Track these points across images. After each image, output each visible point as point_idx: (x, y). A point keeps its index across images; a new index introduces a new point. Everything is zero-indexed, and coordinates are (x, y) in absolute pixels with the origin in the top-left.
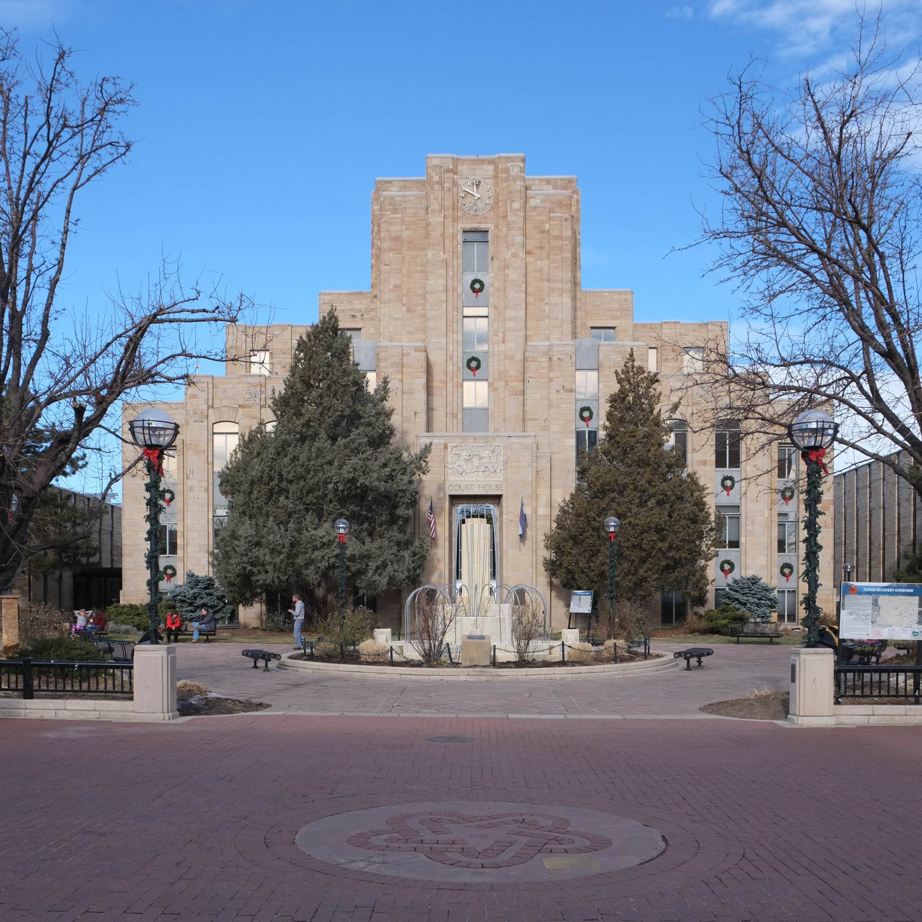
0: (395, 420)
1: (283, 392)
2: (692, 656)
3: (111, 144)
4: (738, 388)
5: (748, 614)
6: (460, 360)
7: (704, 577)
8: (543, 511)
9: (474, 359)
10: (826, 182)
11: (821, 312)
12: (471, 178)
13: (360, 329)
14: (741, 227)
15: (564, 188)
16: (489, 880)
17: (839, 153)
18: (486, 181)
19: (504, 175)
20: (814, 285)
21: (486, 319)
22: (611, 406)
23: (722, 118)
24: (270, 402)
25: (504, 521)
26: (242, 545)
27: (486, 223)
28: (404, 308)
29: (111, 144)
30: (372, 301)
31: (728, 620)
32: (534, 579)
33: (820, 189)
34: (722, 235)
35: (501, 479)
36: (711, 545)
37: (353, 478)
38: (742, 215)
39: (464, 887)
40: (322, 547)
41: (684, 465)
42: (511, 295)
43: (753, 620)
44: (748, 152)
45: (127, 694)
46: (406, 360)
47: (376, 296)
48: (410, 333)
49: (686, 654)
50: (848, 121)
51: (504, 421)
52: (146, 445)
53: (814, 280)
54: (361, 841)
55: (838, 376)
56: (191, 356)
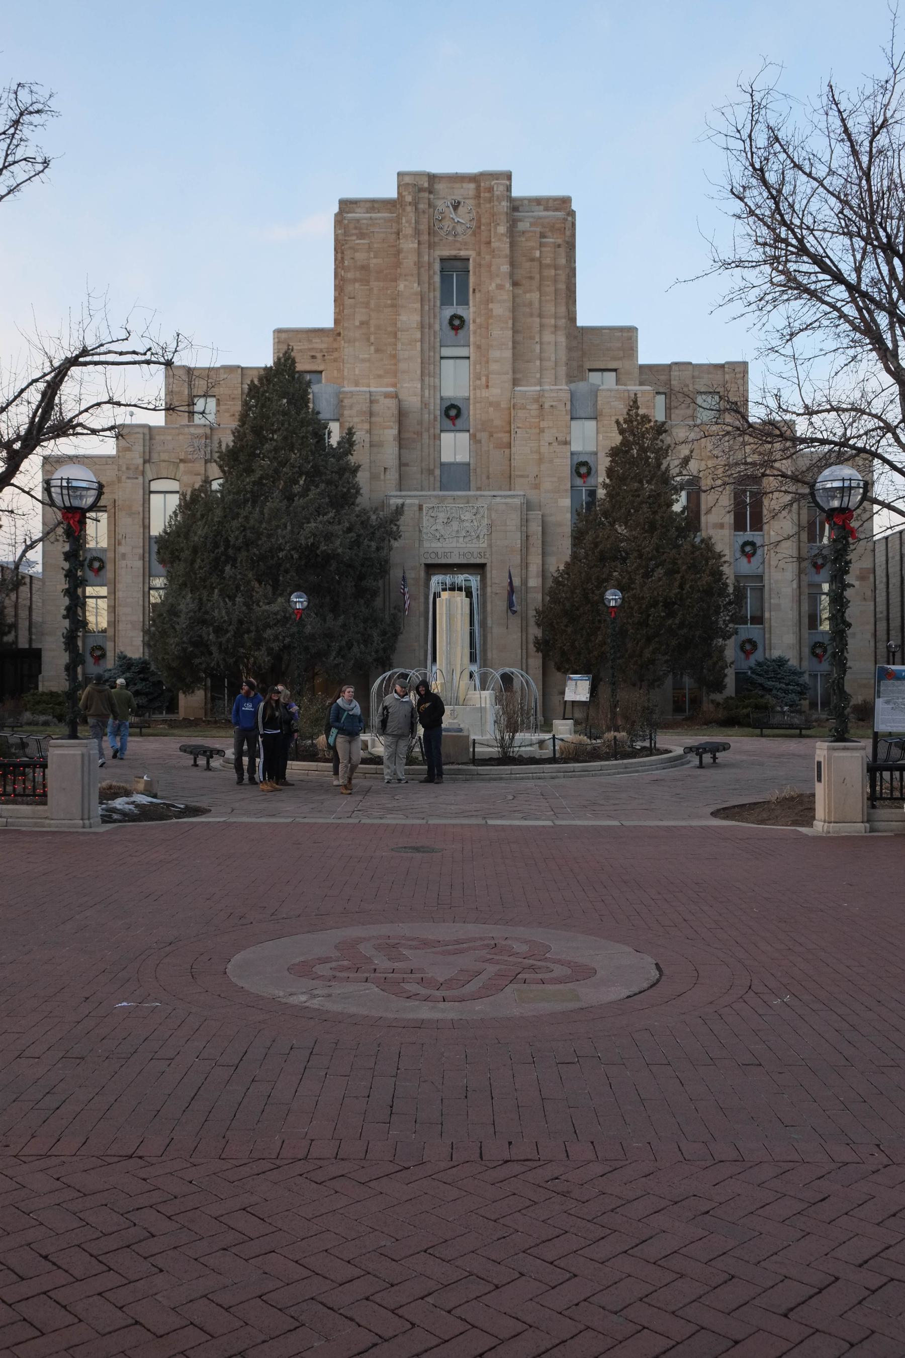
0: (362, 478)
1: (231, 444)
2: (705, 751)
3: (25, 159)
4: (751, 440)
5: (773, 701)
6: (438, 407)
7: (721, 658)
8: (534, 582)
9: (453, 406)
10: (854, 202)
11: (851, 352)
12: (450, 198)
13: (321, 372)
14: (757, 254)
15: (557, 210)
16: (452, 1015)
17: (869, 169)
18: (467, 201)
19: (487, 195)
20: (842, 320)
21: (467, 361)
22: (611, 461)
23: (732, 131)
24: (216, 456)
25: (489, 594)
26: (183, 622)
27: (467, 249)
28: (372, 348)
29: (25, 159)
30: (335, 340)
31: (749, 709)
32: (524, 661)
33: (847, 212)
34: (733, 265)
35: (485, 545)
36: (730, 621)
37: (312, 544)
38: (756, 241)
39: (420, 1025)
40: (275, 625)
41: (698, 529)
42: (496, 332)
43: (779, 709)
44: (761, 170)
45: (40, 797)
46: (376, 408)
47: (339, 334)
48: (380, 376)
49: (698, 749)
50: (878, 133)
51: (488, 478)
52: (65, 508)
53: (842, 316)
54: (304, 970)
55: (870, 426)
56: (119, 404)
